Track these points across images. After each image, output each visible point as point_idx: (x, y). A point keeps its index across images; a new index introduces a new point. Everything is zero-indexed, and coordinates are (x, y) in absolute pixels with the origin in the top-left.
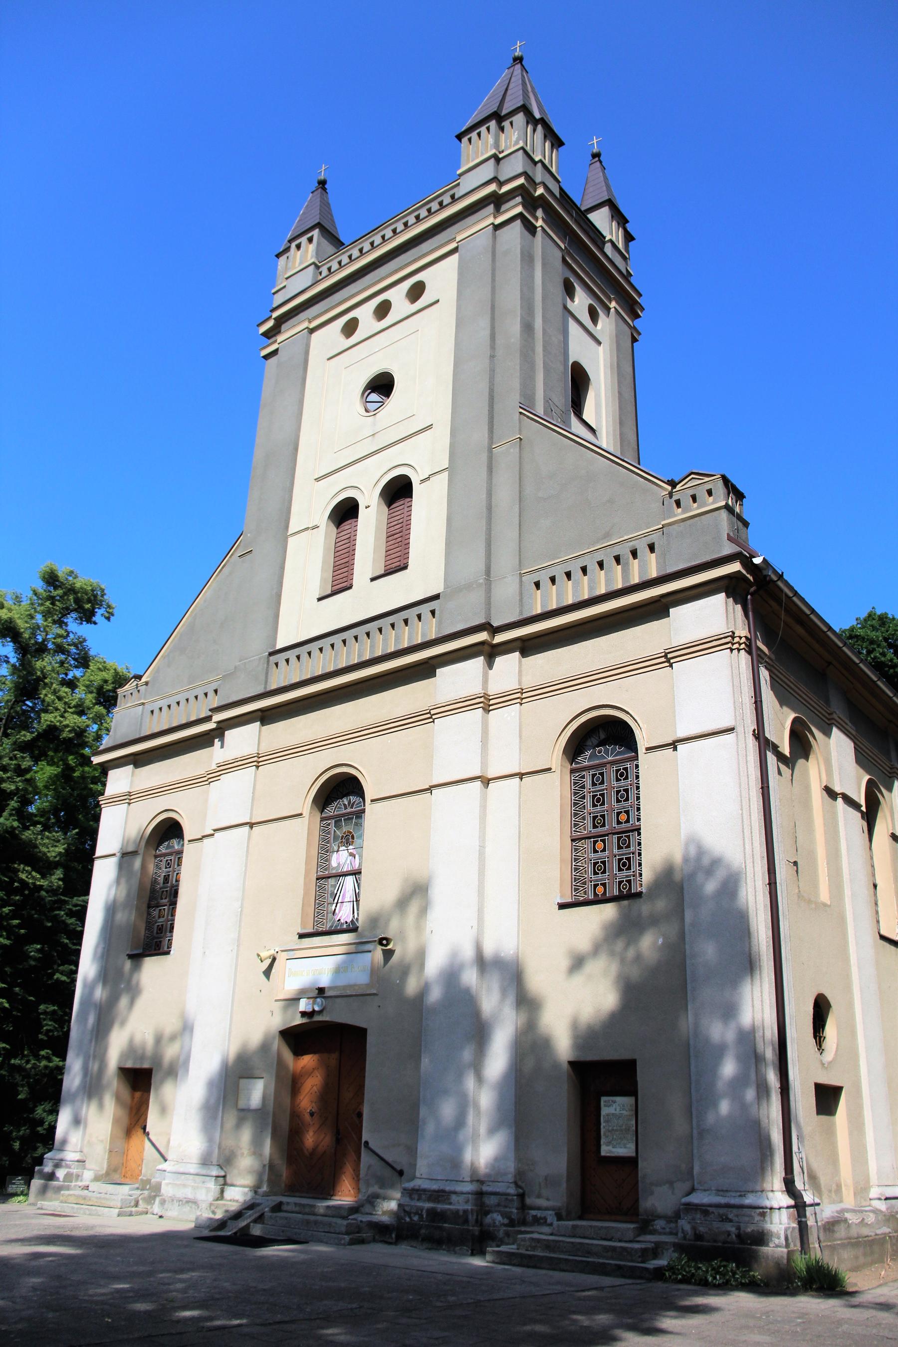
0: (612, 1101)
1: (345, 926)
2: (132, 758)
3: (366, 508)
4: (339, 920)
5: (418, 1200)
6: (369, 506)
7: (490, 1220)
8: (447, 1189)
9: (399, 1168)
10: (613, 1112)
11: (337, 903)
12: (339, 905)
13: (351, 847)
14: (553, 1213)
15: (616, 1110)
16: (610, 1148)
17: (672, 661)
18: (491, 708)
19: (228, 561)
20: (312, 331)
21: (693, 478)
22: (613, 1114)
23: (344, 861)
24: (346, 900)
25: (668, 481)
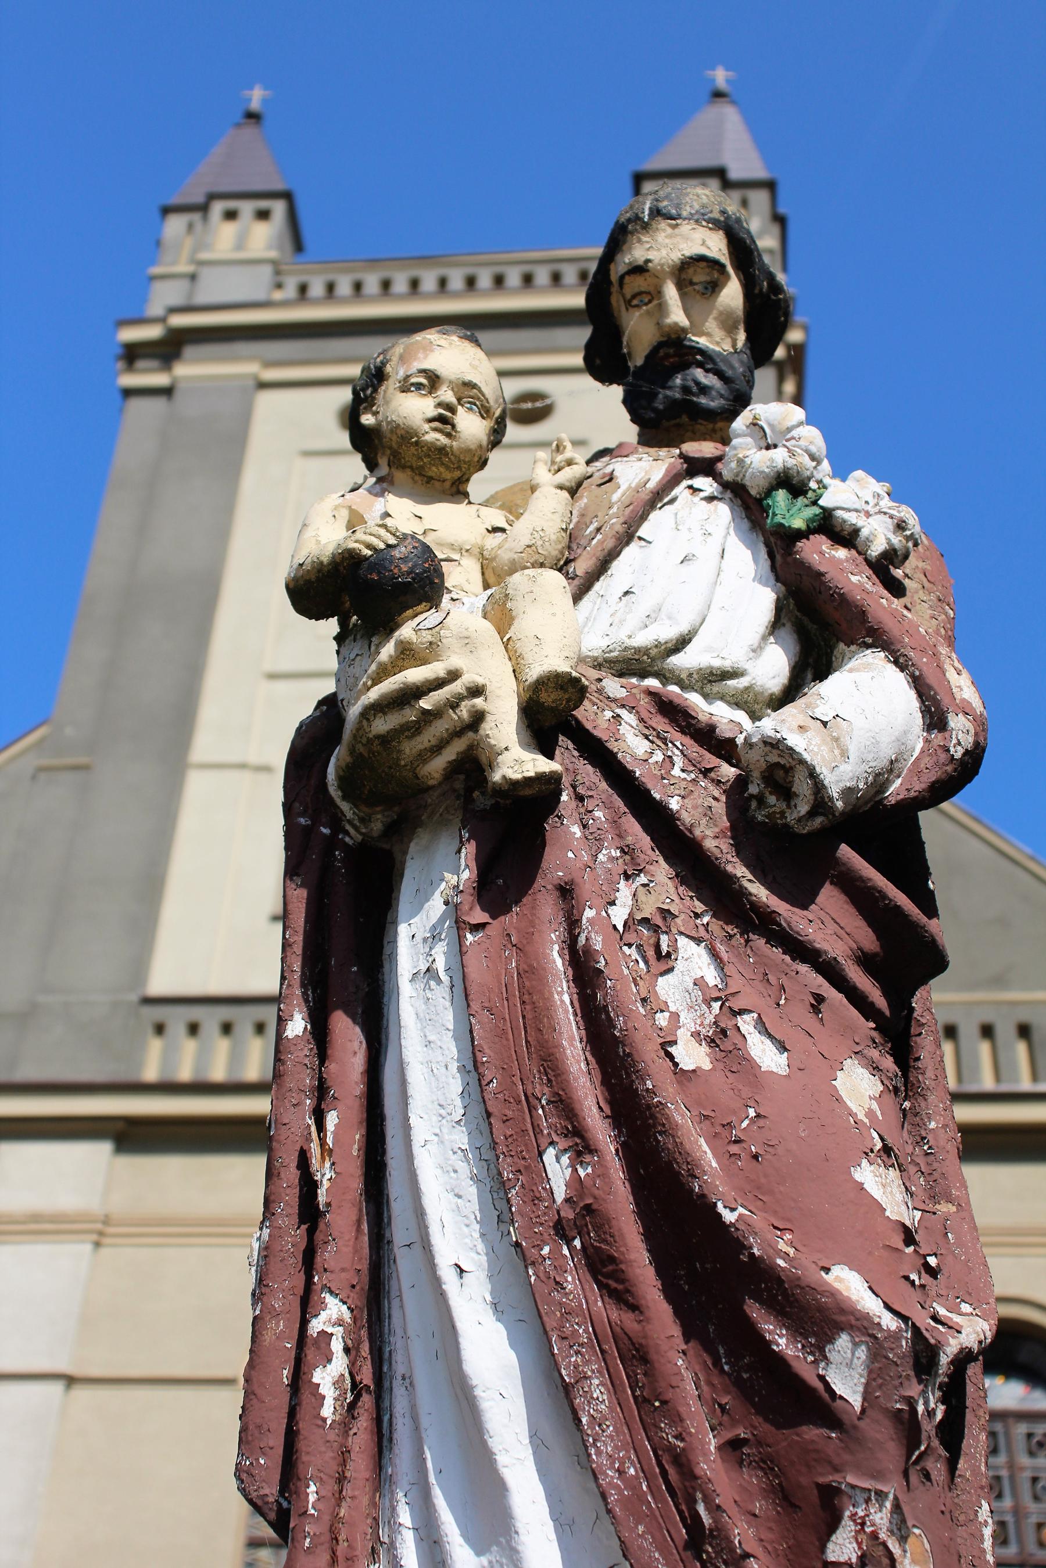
20: (264, 385)
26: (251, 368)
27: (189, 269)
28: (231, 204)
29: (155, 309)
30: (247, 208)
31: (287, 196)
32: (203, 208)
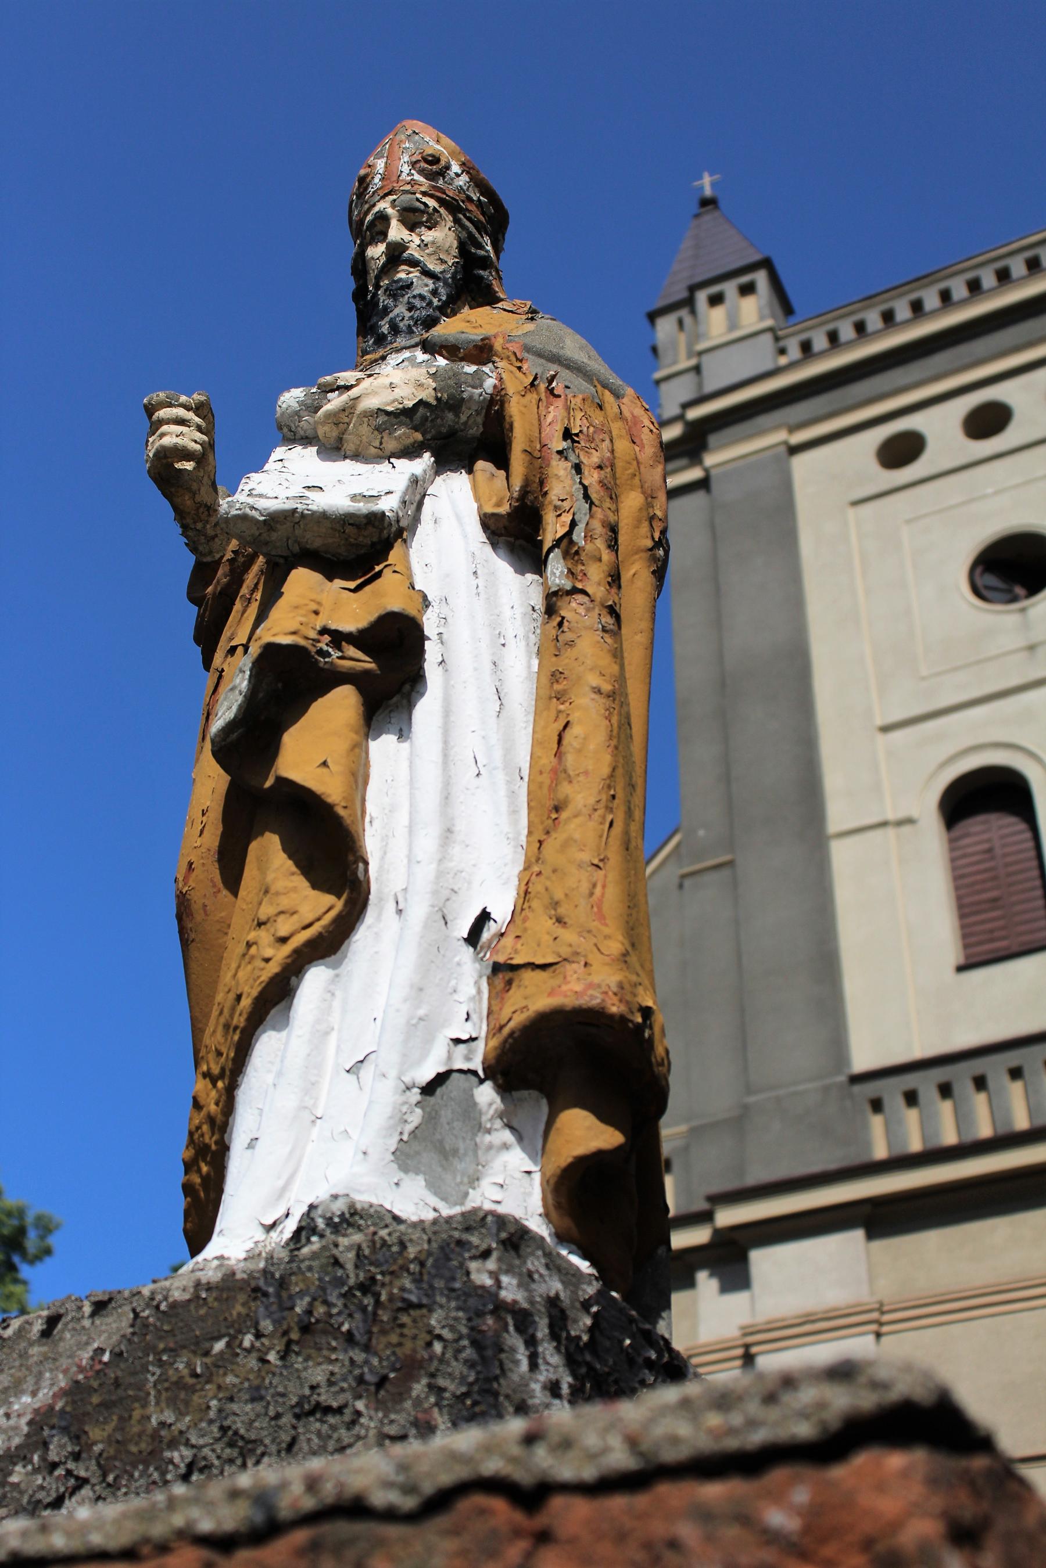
20: (794, 450)
26: (781, 436)
27: (693, 362)
28: (714, 289)
29: (671, 409)
30: (730, 288)
31: (766, 264)
32: (689, 303)
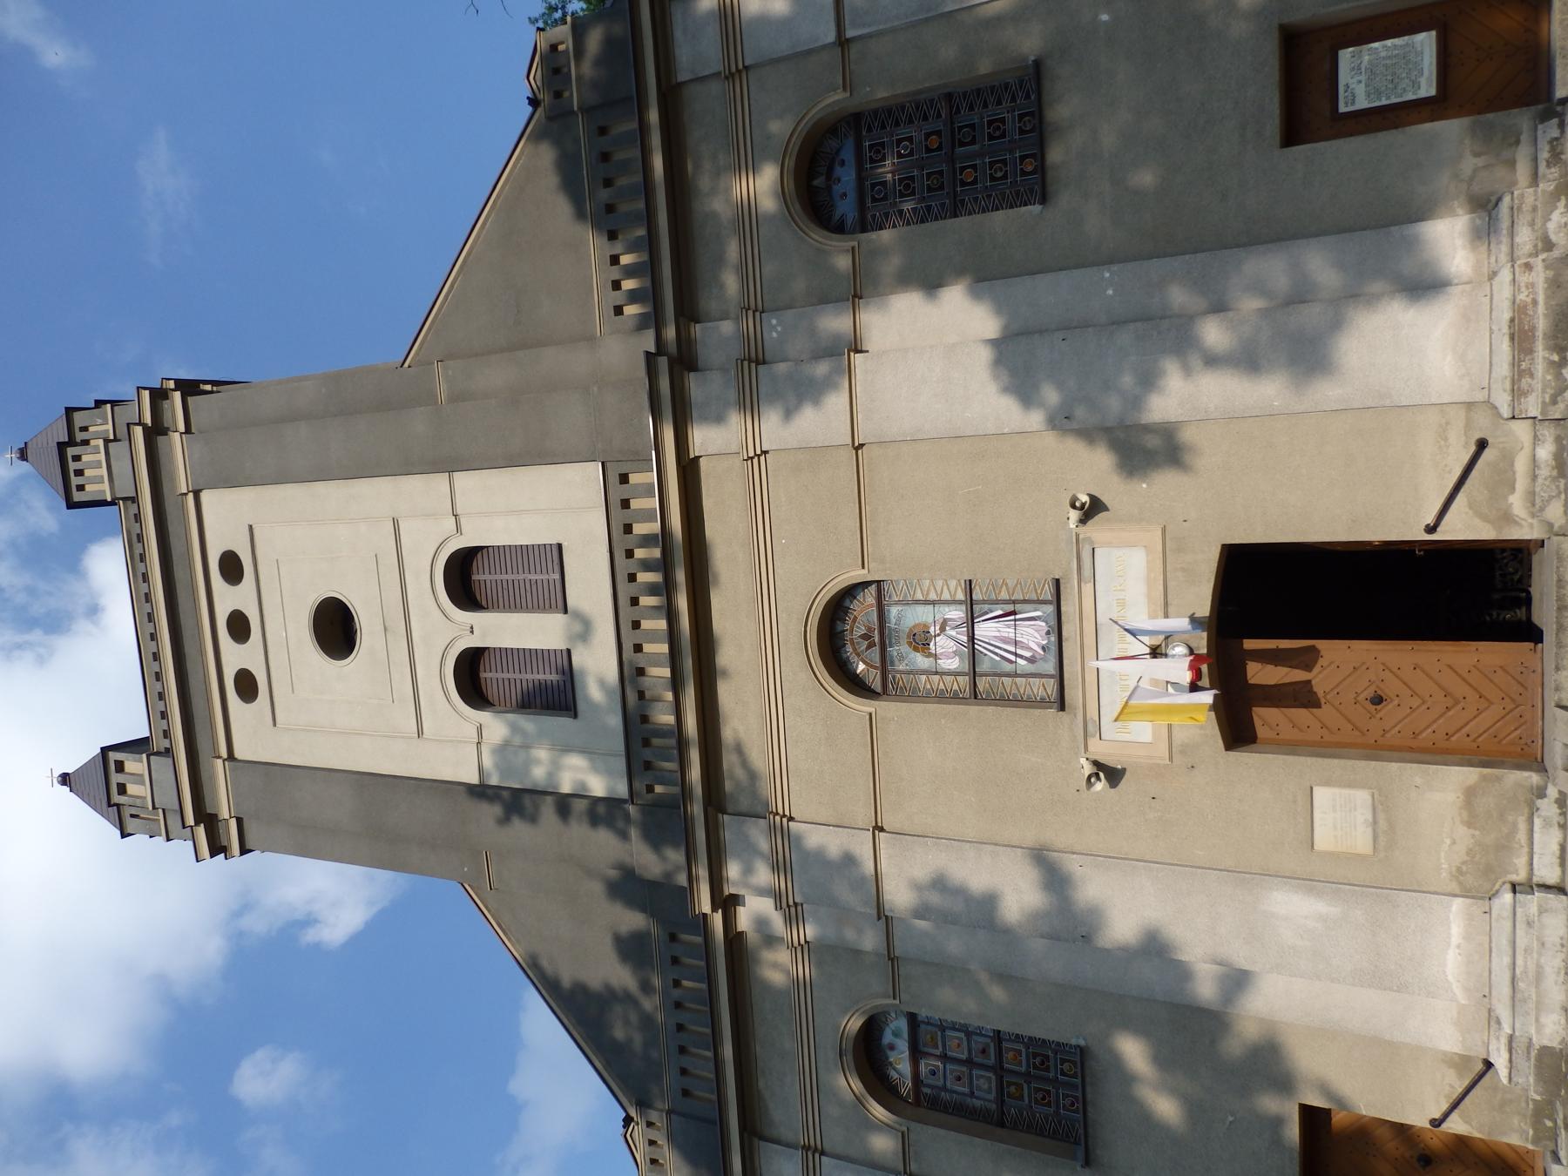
0: (1346, 91)
1: (1053, 639)
2: (746, 1135)
3: (472, 632)
4: (1043, 648)
5: (1532, 376)
6: (472, 628)
7: (1562, 234)
8: (1507, 316)
9: (1473, 448)
10: (1363, 85)
11: (1016, 655)
12: (1019, 652)
13: (932, 630)
14: (1540, 127)
15: (1360, 82)
16: (1423, 81)
17: (741, 66)
18: (761, 356)
19: (492, 916)
21: (631, 1135)
22: (1367, 86)
23: (952, 643)
24: (1012, 635)
25: (624, 1127)
28: (114, 789)
